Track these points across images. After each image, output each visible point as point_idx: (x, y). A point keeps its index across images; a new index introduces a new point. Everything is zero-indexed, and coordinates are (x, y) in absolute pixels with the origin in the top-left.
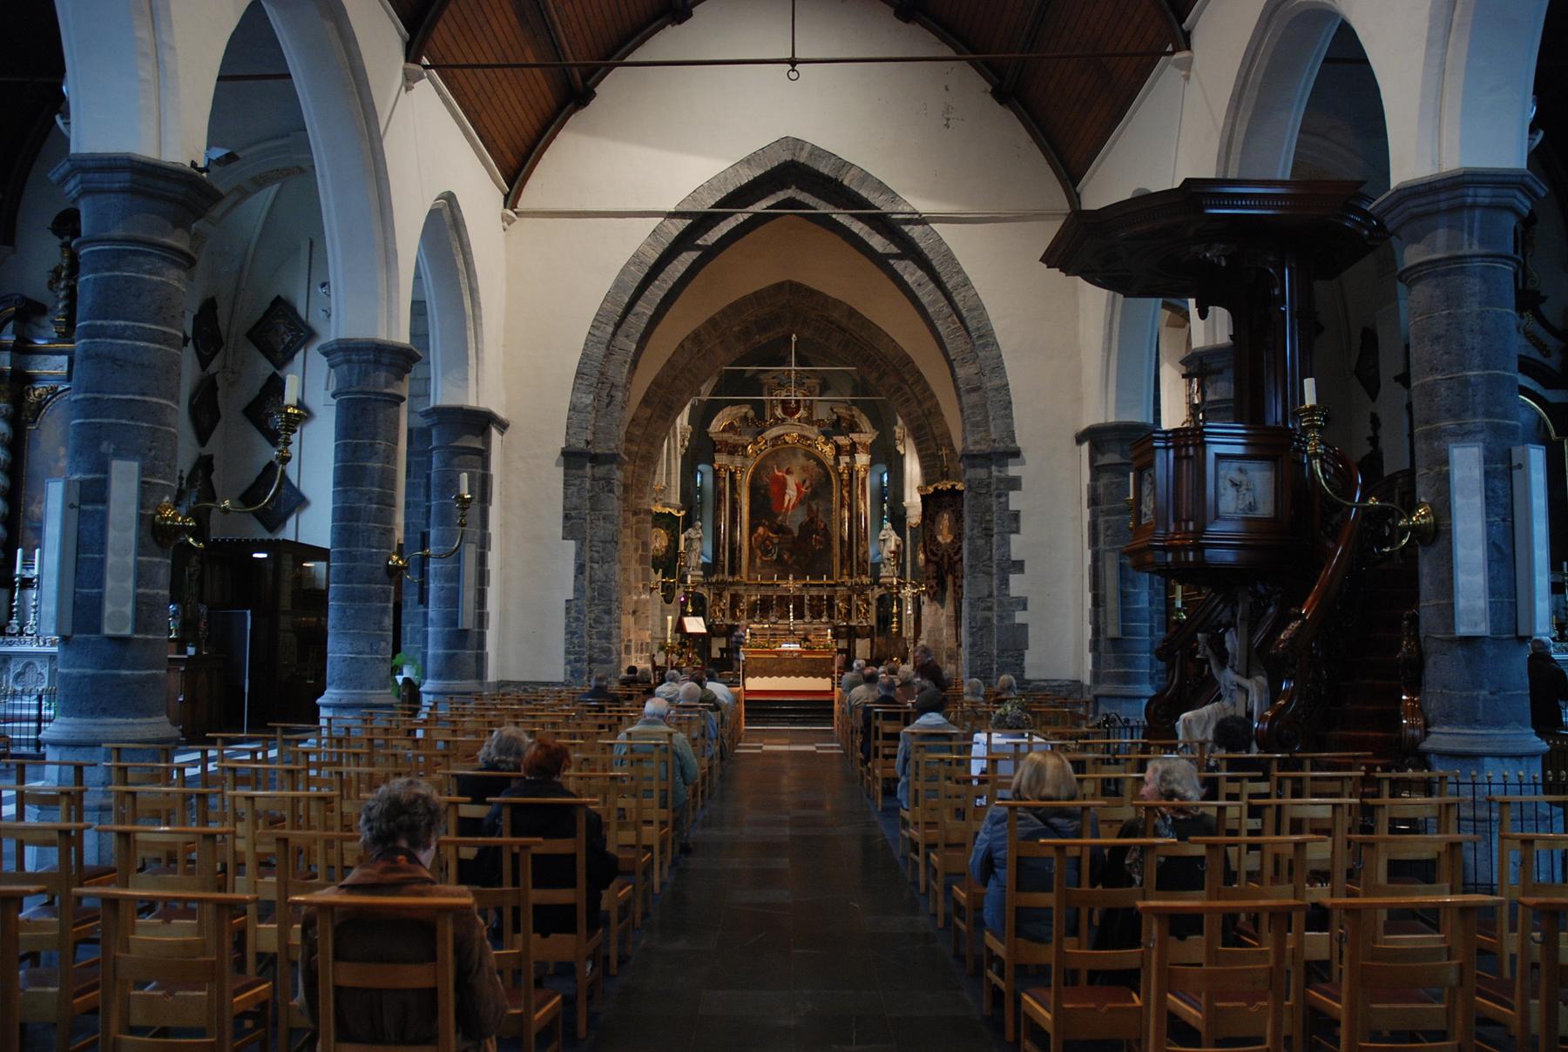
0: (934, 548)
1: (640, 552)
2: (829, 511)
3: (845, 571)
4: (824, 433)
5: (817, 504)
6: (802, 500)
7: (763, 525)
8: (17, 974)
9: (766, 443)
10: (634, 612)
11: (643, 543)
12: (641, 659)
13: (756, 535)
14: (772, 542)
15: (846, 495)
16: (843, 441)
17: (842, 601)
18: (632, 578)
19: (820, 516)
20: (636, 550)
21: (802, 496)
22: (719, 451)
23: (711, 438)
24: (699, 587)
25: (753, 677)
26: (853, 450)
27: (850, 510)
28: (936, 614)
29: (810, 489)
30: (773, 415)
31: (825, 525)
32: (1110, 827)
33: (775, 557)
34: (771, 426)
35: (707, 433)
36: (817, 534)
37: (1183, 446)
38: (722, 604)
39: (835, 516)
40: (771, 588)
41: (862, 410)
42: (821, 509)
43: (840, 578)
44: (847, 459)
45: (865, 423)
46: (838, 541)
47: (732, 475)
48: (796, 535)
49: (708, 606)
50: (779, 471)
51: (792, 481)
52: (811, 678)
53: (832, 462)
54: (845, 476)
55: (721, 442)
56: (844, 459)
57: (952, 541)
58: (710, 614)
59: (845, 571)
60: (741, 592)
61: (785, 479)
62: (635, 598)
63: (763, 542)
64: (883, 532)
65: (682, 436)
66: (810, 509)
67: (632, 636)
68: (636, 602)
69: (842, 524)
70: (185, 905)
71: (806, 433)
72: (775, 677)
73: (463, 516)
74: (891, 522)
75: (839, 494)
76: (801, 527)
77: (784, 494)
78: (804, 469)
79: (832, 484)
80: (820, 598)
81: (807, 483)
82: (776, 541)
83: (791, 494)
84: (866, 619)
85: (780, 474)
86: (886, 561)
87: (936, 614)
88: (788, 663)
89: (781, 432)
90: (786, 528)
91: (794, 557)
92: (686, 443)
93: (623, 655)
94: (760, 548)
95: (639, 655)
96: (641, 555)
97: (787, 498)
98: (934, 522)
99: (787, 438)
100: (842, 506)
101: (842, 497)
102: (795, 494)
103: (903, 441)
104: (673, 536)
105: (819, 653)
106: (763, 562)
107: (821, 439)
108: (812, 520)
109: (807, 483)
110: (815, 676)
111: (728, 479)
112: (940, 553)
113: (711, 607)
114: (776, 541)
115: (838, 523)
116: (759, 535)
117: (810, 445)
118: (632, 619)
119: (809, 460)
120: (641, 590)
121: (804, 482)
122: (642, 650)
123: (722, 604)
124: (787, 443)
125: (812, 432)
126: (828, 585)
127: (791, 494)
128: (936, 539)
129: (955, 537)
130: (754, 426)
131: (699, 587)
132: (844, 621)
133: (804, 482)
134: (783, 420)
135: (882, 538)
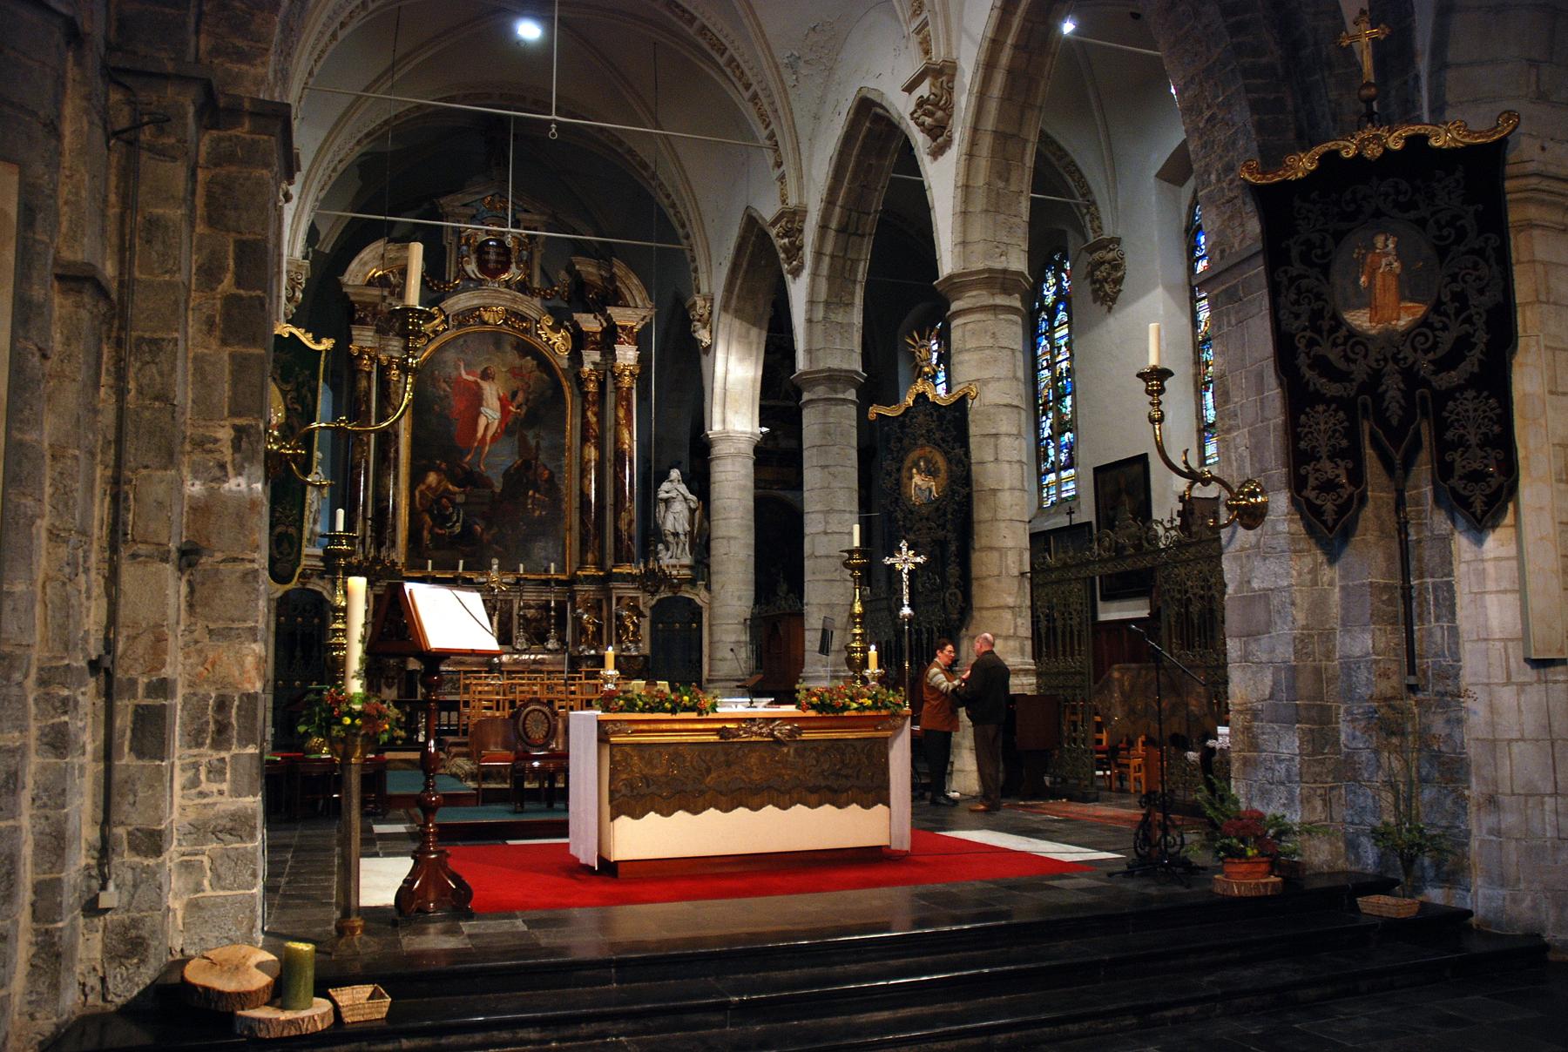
0: (1333, 355)
1: (227, 284)
2: (558, 450)
4: (552, 311)
5: (537, 436)
6: (509, 427)
7: (438, 470)
9: (446, 321)
10: (189, 556)
11: (241, 246)
12: (216, 772)
13: (423, 487)
14: (452, 501)
15: (593, 419)
16: (590, 323)
17: (587, 611)
18: (184, 394)
20: (210, 274)
21: (511, 419)
22: (362, 322)
23: (346, 295)
24: (315, 579)
25: (637, 815)
26: (610, 337)
27: (600, 447)
28: (1314, 583)
29: (524, 408)
30: (461, 273)
31: (552, 475)
33: (457, 529)
34: (456, 291)
35: (340, 285)
36: (537, 490)
39: (570, 461)
41: (633, 267)
42: (543, 444)
43: (579, 569)
44: (596, 356)
45: (633, 286)
46: (576, 503)
47: (383, 371)
48: (498, 490)
50: (468, 374)
51: (492, 393)
52: (827, 809)
53: (565, 364)
54: (592, 387)
55: (365, 306)
56: (591, 357)
57: (1424, 322)
59: (590, 557)
61: (480, 387)
62: (195, 488)
63: (437, 501)
64: (665, 486)
65: (291, 279)
66: (523, 441)
67: (176, 668)
68: (201, 510)
69: (584, 473)
71: (523, 309)
72: (712, 812)
74: (1382, 155)
75: (578, 421)
77: (479, 414)
78: (515, 372)
79: (564, 398)
81: (520, 397)
82: (460, 499)
83: (490, 415)
84: (636, 642)
85: (470, 378)
86: (670, 539)
87: (1314, 583)
88: (753, 760)
89: (476, 302)
90: (480, 475)
91: (495, 530)
92: (299, 295)
93: (126, 760)
94: (430, 512)
95: (208, 754)
96: (230, 301)
97: (482, 422)
98: (1326, 270)
99: (487, 316)
100: (584, 439)
101: (585, 424)
102: (497, 415)
103: (707, 323)
104: (299, 399)
105: (853, 723)
106: (435, 537)
107: (548, 321)
108: (526, 465)
109: (520, 397)
110: (784, 802)
111: (374, 376)
112: (1360, 371)
114: (460, 499)
115: (576, 471)
116: (429, 487)
117: (526, 331)
118: (175, 588)
120: (227, 455)
121: (514, 395)
122: (222, 729)
124: (486, 323)
125: (531, 307)
126: (558, 582)
127: (490, 415)
128: (1338, 323)
129: (1437, 307)
131: (315, 579)
132: (590, 647)
133: (514, 395)
134: (480, 282)
135: (662, 495)
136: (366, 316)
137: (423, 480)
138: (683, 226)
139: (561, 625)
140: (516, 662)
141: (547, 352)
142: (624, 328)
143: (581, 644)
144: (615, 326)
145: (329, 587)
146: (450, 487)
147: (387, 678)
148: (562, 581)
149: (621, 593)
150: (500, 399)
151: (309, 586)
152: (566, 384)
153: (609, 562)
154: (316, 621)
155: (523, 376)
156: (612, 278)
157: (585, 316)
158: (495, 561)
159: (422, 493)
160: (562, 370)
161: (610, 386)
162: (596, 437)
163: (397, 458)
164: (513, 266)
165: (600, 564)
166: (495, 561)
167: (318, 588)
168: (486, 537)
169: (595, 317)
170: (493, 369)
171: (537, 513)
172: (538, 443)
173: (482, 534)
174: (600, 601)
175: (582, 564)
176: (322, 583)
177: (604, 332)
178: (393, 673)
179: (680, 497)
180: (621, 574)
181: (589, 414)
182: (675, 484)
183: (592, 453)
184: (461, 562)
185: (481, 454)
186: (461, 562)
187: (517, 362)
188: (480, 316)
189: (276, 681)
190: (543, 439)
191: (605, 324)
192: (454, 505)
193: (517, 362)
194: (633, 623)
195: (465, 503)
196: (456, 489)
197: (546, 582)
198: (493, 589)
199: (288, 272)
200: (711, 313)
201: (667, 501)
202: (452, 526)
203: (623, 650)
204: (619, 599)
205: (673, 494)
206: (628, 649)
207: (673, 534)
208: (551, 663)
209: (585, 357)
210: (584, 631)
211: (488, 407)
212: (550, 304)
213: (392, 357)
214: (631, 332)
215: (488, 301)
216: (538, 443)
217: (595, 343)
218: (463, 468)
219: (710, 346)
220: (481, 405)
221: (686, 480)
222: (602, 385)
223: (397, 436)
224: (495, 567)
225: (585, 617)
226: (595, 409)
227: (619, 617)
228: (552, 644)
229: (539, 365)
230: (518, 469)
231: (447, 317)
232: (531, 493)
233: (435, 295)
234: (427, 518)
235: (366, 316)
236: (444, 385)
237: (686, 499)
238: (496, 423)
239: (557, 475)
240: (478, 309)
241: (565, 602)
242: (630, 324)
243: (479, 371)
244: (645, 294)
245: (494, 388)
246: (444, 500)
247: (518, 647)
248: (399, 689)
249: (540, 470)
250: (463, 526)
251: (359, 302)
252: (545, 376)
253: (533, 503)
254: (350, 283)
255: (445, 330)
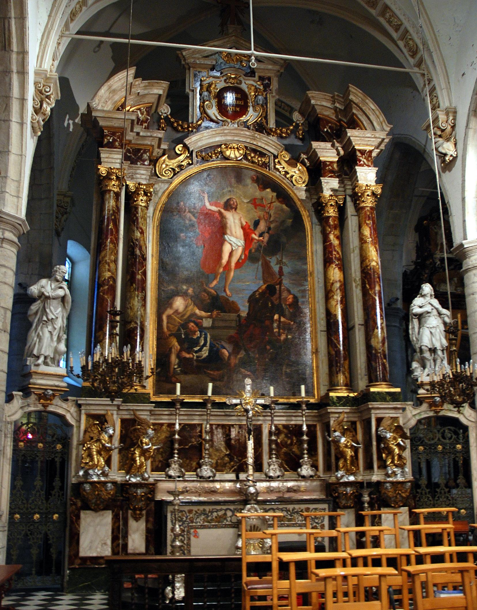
3: (341, 378)
4: (288, 148)
5: (279, 262)
7: (184, 295)
8: (308, 445)
13: (169, 312)
17: (343, 434)
19: (286, 282)
21: (254, 246)
22: (111, 145)
24: (57, 401)
27: (344, 267)
29: (266, 237)
31: (295, 298)
32: (22, 423)
33: (205, 353)
36: (282, 314)
37: (237, 477)
38: (105, 437)
40: (198, 411)
47: (130, 197)
48: (244, 314)
49: (75, 442)
54: (332, 212)
58: (79, 458)
59: (341, 378)
60: (144, 416)
63: (185, 326)
64: (418, 301)
65: (39, 92)
66: (267, 268)
69: (328, 295)
70: (237, 477)
73: (346, 594)
76: (252, 300)
78: (255, 203)
80: (297, 430)
81: (262, 226)
82: (207, 323)
84: (402, 466)
85: (214, 208)
86: (427, 355)
91: (242, 354)
94: (178, 336)
97: (227, 249)
100: (327, 262)
101: (327, 248)
102: (241, 243)
106: (183, 362)
108: (271, 290)
109: (262, 226)
113: (82, 443)
114: (207, 323)
115: (320, 295)
116: (176, 312)
117: (265, 165)
119: (265, 188)
121: (256, 224)
123: (105, 437)
126: (310, 406)
130: (169, 129)
131: (57, 401)
132: (349, 472)
133: (256, 224)
136: (114, 141)
137: (170, 305)
138: (414, 53)
139: (313, 451)
140: (270, 490)
141: (285, 184)
142: (363, 152)
143: (337, 469)
144: (354, 150)
145: (73, 409)
146: (197, 311)
147: (135, 510)
148: (312, 404)
149: (380, 414)
150: (243, 228)
151: (51, 409)
152: (305, 214)
153: (362, 383)
154: (59, 447)
155: (264, 206)
156: (349, 105)
157: (322, 144)
158: (248, 381)
159: (169, 317)
160: (301, 200)
161: (350, 209)
162: (338, 259)
163: (144, 281)
164: (251, 109)
165: (350, 386)
166: (248, 381)
167: (61, 411)
168: (234, 361)
169: (333, 146)
170: (236, 200)
171: (283, 337)
172: (281, 269)
173: (229, 358)
174: (354, 423)
175: (332, 386)
176: (64, 405)
177: (342, 161)
178: (141, 504)
179: (435, 312)
180: (379, 393)
181: (332, 237)
182: (428, 298)
183: (335, 274)
184: (210, 385)
185: (226, 279)
186: (210, 385)
187: (258, 194)
188: (221, 152)
189: (11, 513)
190: (286, 265)
191: (342, 152)
192: (202, 329)
193: (258, 194)
194: (398, 445)
195: (213, 327)
196: (203, 314)
197: (297, 406)
198: (247, 411)
199: (36, 83)
200: (453, 127)
201: (420, 317)
202: (200, 350)
203: (388, 476)
204: (379, 420)
205: (428, 308)
206: (394, 474)
207: (430, 350)
208: (306, 491)
209: (324, 185)
210: (340, 455)
211: (232, 235)
212: (286, 142)
213: (139, 184)
214: (370, 156)
215: (229, 138)
216: (281, 269)
217: (332, 171)
218: (208, 293)
219: (455, 159)
220: (225, 233)
221: (439, 296)
222: (341, 210)
223: (145, 259)
224: (248, 388)
225: (343, 440)
226: (337, 232)
227: (380, 439)
228: (306, 470)
229: (278, 197)
230: (263, 294)
231: (191, 153)
232: (276, 317)
233: (179, 135)
234: (175, 344)
235: (114, 141)
236: (189, 215)
237: (440, 314)
238: (240, 250)
239: (300, 300)
240: (220, 146)
241: (315, 426)
242: (368, 148)
243: (222, 201)
244: (382, 118)
245: (237, 217)
246: (191, 325)
247: (271, 474)
248: (147, 522)
249: (285, 294)
250: (210, 351)
251: (107, 127)
252: (284, 206)
253: (279, 327)
254: (99, 108)
255: (189, 164)
